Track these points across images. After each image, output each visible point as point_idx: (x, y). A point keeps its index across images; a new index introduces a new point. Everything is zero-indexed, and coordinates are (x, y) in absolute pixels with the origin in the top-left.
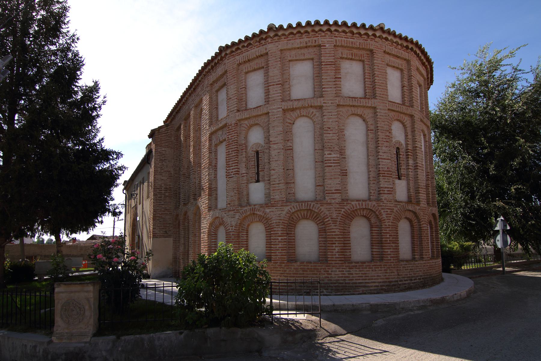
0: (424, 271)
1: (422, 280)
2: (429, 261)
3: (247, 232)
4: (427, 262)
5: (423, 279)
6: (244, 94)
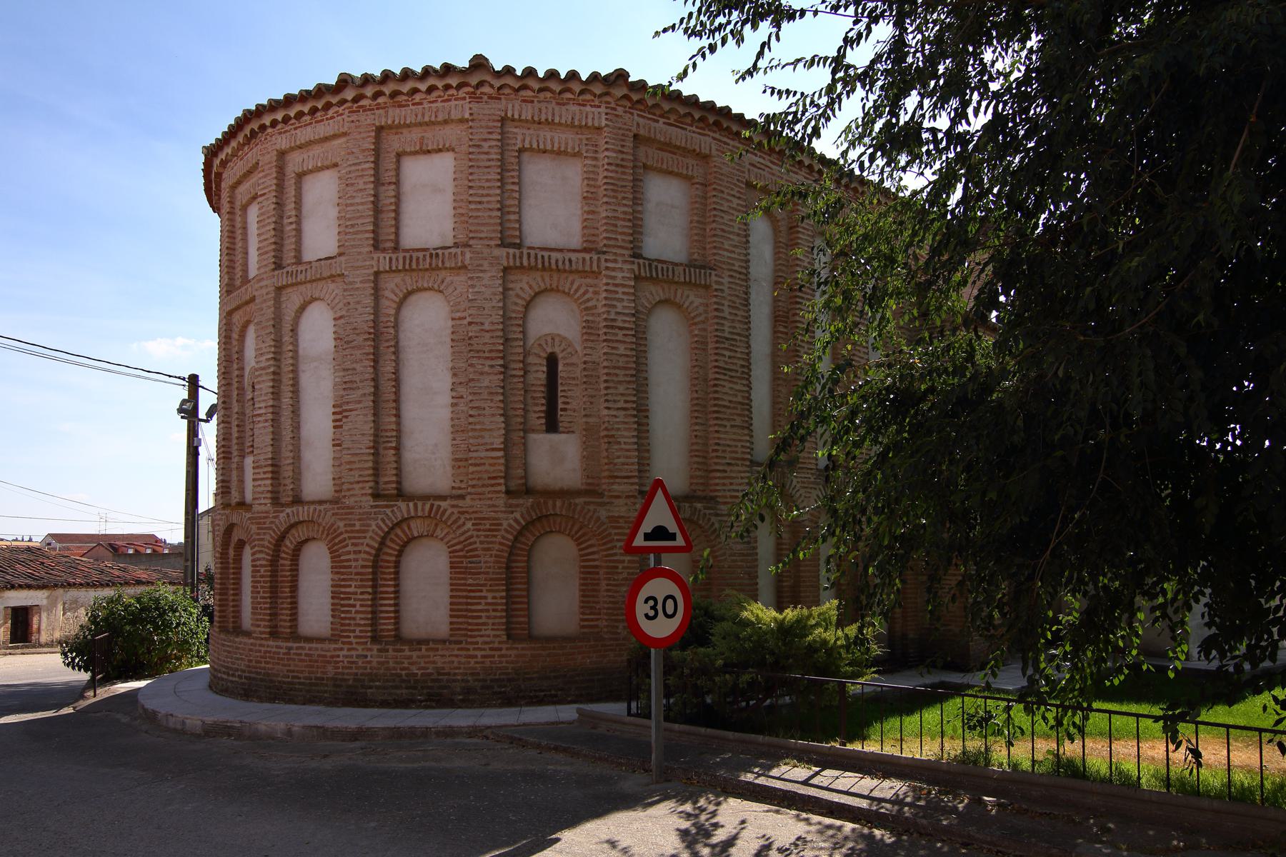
0: (250, 661)
1: (243, 680)
2: (264, 642)
3: (396, 598)
4: (258, 642)
5: (246, 678)
6: (532, 252)
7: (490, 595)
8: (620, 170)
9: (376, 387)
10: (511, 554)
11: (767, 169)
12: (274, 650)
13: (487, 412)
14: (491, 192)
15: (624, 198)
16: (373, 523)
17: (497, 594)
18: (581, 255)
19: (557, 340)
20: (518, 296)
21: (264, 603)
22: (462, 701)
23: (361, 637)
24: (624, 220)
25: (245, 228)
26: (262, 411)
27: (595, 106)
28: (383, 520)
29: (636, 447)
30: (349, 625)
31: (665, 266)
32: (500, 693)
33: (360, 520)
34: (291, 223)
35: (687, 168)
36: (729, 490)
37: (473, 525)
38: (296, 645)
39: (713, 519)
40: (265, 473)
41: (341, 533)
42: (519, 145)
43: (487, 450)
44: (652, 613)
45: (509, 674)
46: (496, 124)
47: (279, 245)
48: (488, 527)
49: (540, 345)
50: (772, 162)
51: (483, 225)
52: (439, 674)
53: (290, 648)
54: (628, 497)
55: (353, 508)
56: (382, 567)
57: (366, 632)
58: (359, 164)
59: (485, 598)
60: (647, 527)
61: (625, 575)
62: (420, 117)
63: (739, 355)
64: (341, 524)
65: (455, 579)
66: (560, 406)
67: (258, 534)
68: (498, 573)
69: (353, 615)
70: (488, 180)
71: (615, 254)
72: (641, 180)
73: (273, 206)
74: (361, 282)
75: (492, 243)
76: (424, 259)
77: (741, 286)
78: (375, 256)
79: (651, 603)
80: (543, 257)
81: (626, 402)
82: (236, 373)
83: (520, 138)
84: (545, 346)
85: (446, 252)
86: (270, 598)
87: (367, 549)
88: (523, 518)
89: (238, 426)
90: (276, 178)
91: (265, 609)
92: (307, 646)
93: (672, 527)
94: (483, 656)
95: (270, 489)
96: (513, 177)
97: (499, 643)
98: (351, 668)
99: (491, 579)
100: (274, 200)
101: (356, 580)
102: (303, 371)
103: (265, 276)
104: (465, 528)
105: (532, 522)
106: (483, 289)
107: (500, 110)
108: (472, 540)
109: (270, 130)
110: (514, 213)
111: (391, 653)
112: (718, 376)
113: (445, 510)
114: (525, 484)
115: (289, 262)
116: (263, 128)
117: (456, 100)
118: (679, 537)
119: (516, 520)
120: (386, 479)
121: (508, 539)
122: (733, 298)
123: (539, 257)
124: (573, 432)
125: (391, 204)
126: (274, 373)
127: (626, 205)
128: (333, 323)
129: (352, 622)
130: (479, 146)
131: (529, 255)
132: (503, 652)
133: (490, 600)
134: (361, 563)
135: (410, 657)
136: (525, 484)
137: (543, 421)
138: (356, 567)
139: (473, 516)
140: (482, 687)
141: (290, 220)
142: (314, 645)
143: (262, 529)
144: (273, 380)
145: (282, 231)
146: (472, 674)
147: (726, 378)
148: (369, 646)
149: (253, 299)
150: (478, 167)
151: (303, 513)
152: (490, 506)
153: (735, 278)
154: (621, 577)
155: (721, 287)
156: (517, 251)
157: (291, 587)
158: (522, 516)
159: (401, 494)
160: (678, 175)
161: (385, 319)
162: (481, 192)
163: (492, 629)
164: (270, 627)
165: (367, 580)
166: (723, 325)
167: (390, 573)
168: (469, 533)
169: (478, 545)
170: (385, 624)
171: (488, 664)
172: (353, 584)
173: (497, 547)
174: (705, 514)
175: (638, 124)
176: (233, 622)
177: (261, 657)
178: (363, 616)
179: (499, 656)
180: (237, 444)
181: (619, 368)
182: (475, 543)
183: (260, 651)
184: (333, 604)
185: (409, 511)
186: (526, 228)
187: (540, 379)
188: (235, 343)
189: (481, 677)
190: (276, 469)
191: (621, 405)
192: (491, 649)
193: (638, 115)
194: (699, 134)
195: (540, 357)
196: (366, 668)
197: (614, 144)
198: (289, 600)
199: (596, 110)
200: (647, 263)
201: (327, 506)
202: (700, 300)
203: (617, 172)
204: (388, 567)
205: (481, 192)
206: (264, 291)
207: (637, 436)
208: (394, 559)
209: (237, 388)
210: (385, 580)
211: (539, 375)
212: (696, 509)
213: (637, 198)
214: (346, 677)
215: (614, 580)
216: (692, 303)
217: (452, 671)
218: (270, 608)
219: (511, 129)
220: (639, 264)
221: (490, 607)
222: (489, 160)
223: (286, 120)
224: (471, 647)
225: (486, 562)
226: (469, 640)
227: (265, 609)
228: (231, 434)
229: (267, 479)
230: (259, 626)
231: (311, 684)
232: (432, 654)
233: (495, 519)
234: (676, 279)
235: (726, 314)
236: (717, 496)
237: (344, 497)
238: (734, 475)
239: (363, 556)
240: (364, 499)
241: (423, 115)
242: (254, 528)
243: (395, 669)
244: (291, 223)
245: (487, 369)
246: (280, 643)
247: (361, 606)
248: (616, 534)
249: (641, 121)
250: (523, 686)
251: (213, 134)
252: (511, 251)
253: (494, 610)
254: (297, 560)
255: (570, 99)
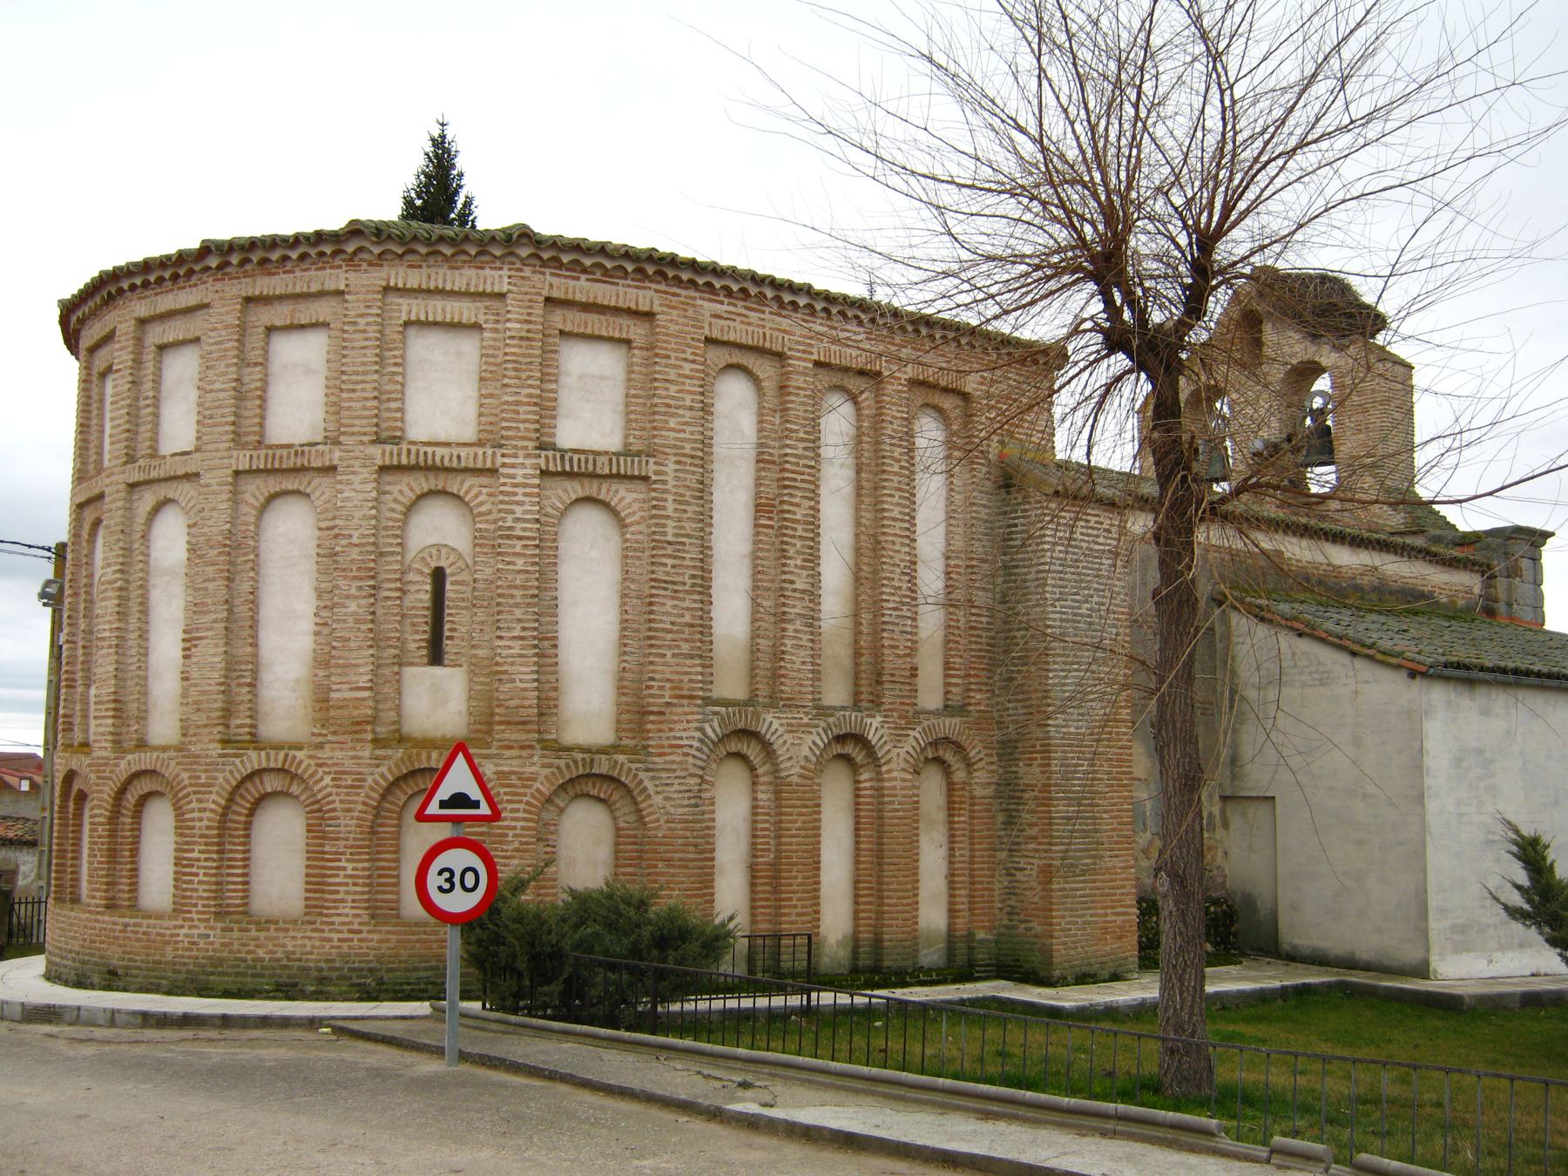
0: (84, 940)
2: (99, 917)
6: (413, 448)
7: (350, 866)
8: (525, 343)
9: (230, 611)
10: (377, 816)
11: (739, 319)
12: (110, 926)
13: (353, 645)
14: (368, 378)
15: (529, 377)
16: (220, 775)
17: (360, 865)
18: (471, 450)
19: (444, 551)
20: (395, 500)
21: (102, 869)
22: (314, 992)
23: (204, 913)
24: (529, 404)
25: (102, 401)
26: (107, 634)
27: (496, 268)
28: (231, 772)
29: (536, 684)
30: (190, 897)
31: (583, 457)
32: (358, 985)
33: (206, 771)
34: (148, 406)
35: (621, 330)
36: (668, 738)
37: (333, 779)
38: (132, 921)
39: (642, 775)
40: (107, 710)
41: (185, 787)
42: (404, 318)
43: (351, 689)
44: (447, 886)
45: (370, 961)
46: (375, 296)
47: (132, 433)
48: (349, 782)
49: (423, 558)
50: (746, 308)
51: (357, 417)
52: (289, 959)
53: (126, 925)
54: (522, 747)
55: (199, 757)
56: (230, 829)
57: (209, 906)
58: (220, 343)
59: (344, 869)
60: (444, 792)
61: (516, 845)
62: (290, 287)
63: (687, 563)
64: (185, 775)
65: (312, 845)
66: (447, 633)
67: (98, 785)
68: (360, 839)
69: (196, 886)
70: (363, 364)
71: (515, 447)
72: (556, 352)
73: (128, 386)
74: (218, 484)
75: (366, 439)
76: (289, 458)
77: (693, 473)
78: (235, 454)
79: (447, 875)
80: (425, 453)
81: (524, 629)
82: (84, 581)
83: (405, 309)
84: (429, 560)
85: (313, 449)
86: (108, 863)
87: (213, 806)
88: (391, 773)
89: (84, 647)
90: (132, 352)
91: (102, 876)
92: (145, 922)
93: (475, 793)
94: (339, 940)
95: (111, 729)
96: (395, 357)
97: (360, 924)
98: (191, 950)
99: (351, 847)
100: (130, 379)
101: (200, 844)
102: (154, 586)
103: (115, 470)
104: (323, 783)
105: (405, 777)
106: (352, 494)
107: (380, 279)
108: (330, 799)
109: (129, 294)
110: (396, 400)
111: (236, 934)
112: (654, 591)
113: (301, 762)
114: (398, 731)
115: (143, 453)
116: (121, 291)
117: (331, 268)
118: (483, 804)
119: (382, 775)
120: (239, 722)
121: (371, 798)
122: (681, 491)
123: (421, 453)
124: (460, 666)
125: (257, 388)
126: (121, 589)
127: (531, 386)
128: (187, 530)
129: (195, 894)
130: (354, 323)
131: (409, 451)
132: (364, 935)
133: (350, 872)
134: (205, 823)
135: (256, 939)
136: (398, 731)
137: (424, 652)
138: (200, 829)
139: (332, 770)
140: (339, 978)
141: (147, 402)
142: (152, 921)
143: (102, 778)
144: (119, 597)
145: (138, 417)
146: (327, 961)
147: (668, 593)
148: (212, 923)
149: (101, 496)
150: (353, 348)
151: (145, 760)
152: (353, 758)
153: (685, 464)
154: (511, 847)
155: (663, 478)
156: (395, 448)
157: (131, 850)
158: (390, 769)
159: (255, 742)
160: (610, 340)
161: (244, 528)
162: (354, 378)
163: (352, 907)
164: (106, 899)
165: (212, 844)
166: (664, 526)
167: (239, 836)
168: (329, 790)
169: (337, 805)
170: (232, 898)
171: (345, 949)
172: (197, 848)
173: (360, 807)
174: (630, 770)
175: (551, 285)
176: (71, 893)
177: (97, 935)
178: (206, 887)
179: (359, 940)
180: (83, 670)
181: (516, 587)
182: (334, 802)
183: (95, 929)
184: (175, 873)
185: (260, 761)
186: (410, 416)
187: (421, 601)
188: (85, 544)
189: (338, 965)
190: (118, 705)
191: (517, 633)
192: (350, 931)
193: (552, 274)
194: (637, 287)
195: (422, 573)
196: (207, 951)
197: (518, 313)
198: (129, 866)
199: (496, 273)
200: (558, 455)
201: (172, 754)
202: (635, 495)
203: (521, 347)
204: (237, 829)
205: (354, 378)
206: (114, 488)
207: (537, 672)
208: (243, 819)
209: (85, 601)
210: (234, 844)
211: (421, 595)
212: (616, 762)
213: (548, 373)
214: (186, 960)
215: (503, 850)
216: (622, 499)
217: (304, 957)
218: (107, 876)
219: (394, 299)
220: (547, 457)
221: (350, 881)
222: (367, 339)
223: (146, 285)
224: (326, 928)
225: (346, 826)
226: (325, 919)
227: (102, 876)
228: (76, 657)
229: (108, 717)
230: (94, 897)
231: (148, 969)
232: (281, 934)
233: (360, 774)
234: (599, 471)
235: (670, 512)
236: (649, 746)
237: (190, 743)
238: (676, 718)
239: (208, 814)
240: (212, 746)
241: (294, 284)
242: (93, 776)
243: (239, 951)
244: (148, 406)
245: (353, 591)
246: (116, 919)
247: (205, 874)
248: (505, 794)
249: (555, 281)
250: (386, 978)
251: (71, 289)
252: (388, 448)
253: (355, 884)
254: (140, 817)
255: (465, 261)
